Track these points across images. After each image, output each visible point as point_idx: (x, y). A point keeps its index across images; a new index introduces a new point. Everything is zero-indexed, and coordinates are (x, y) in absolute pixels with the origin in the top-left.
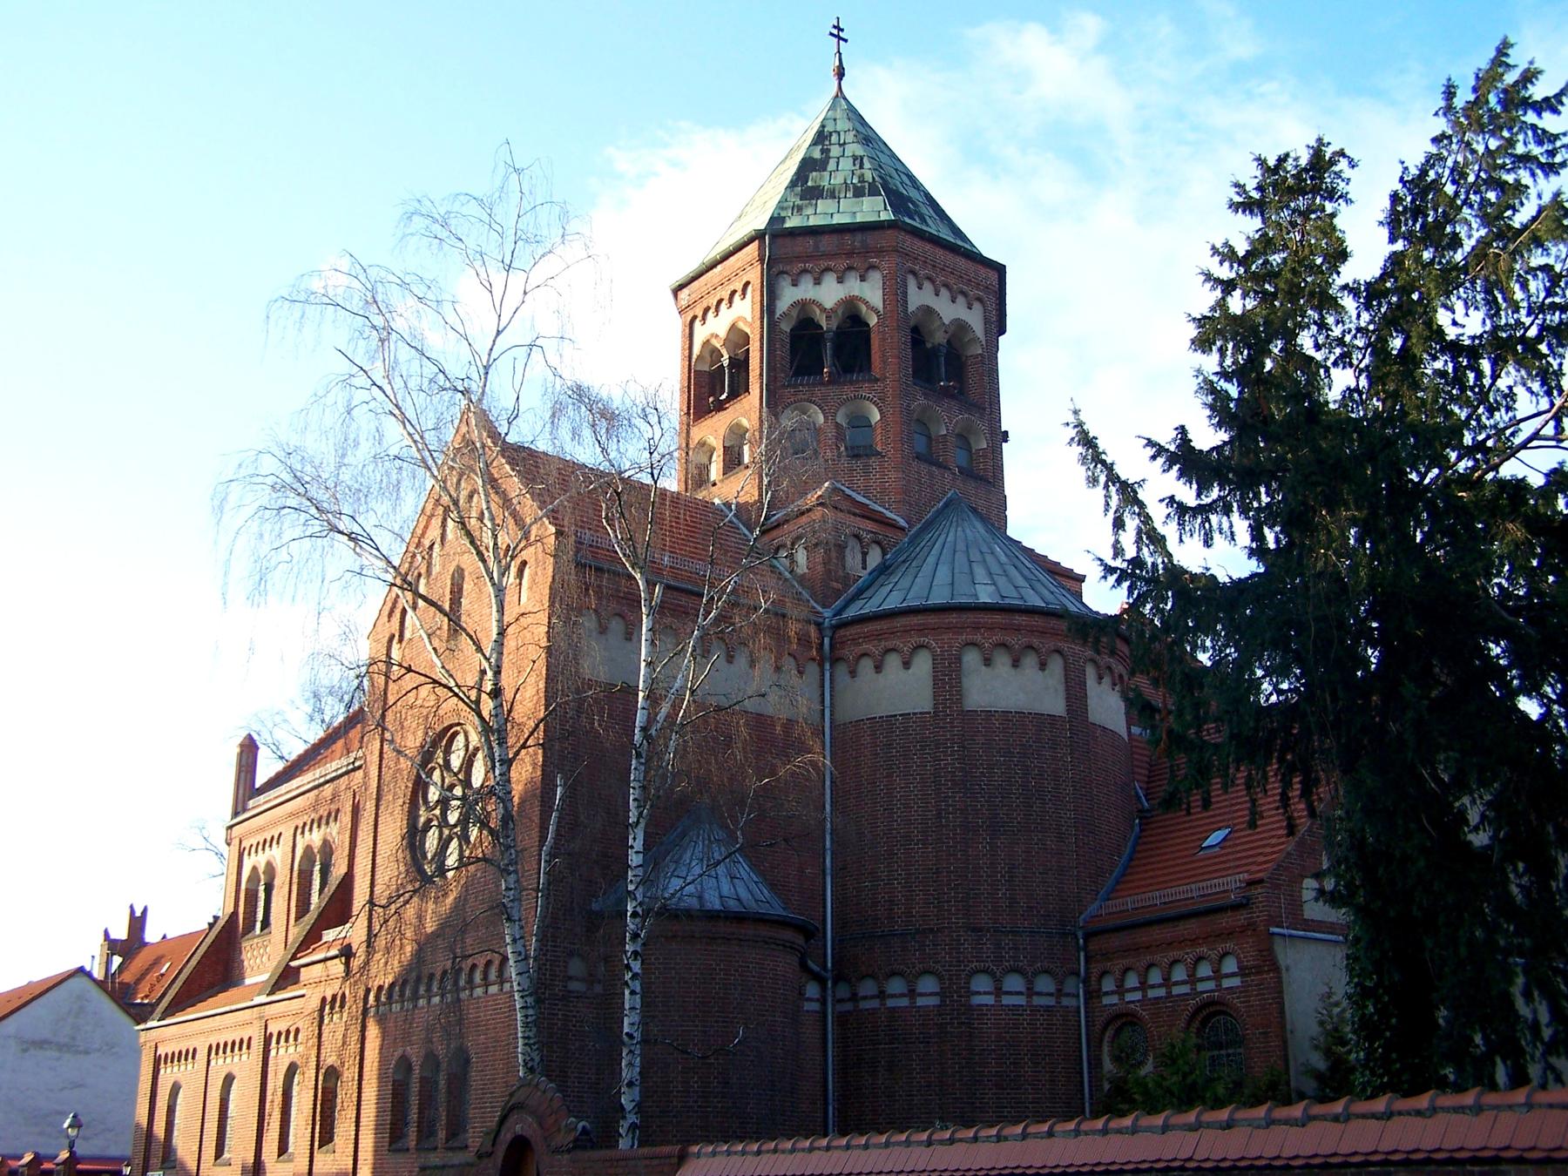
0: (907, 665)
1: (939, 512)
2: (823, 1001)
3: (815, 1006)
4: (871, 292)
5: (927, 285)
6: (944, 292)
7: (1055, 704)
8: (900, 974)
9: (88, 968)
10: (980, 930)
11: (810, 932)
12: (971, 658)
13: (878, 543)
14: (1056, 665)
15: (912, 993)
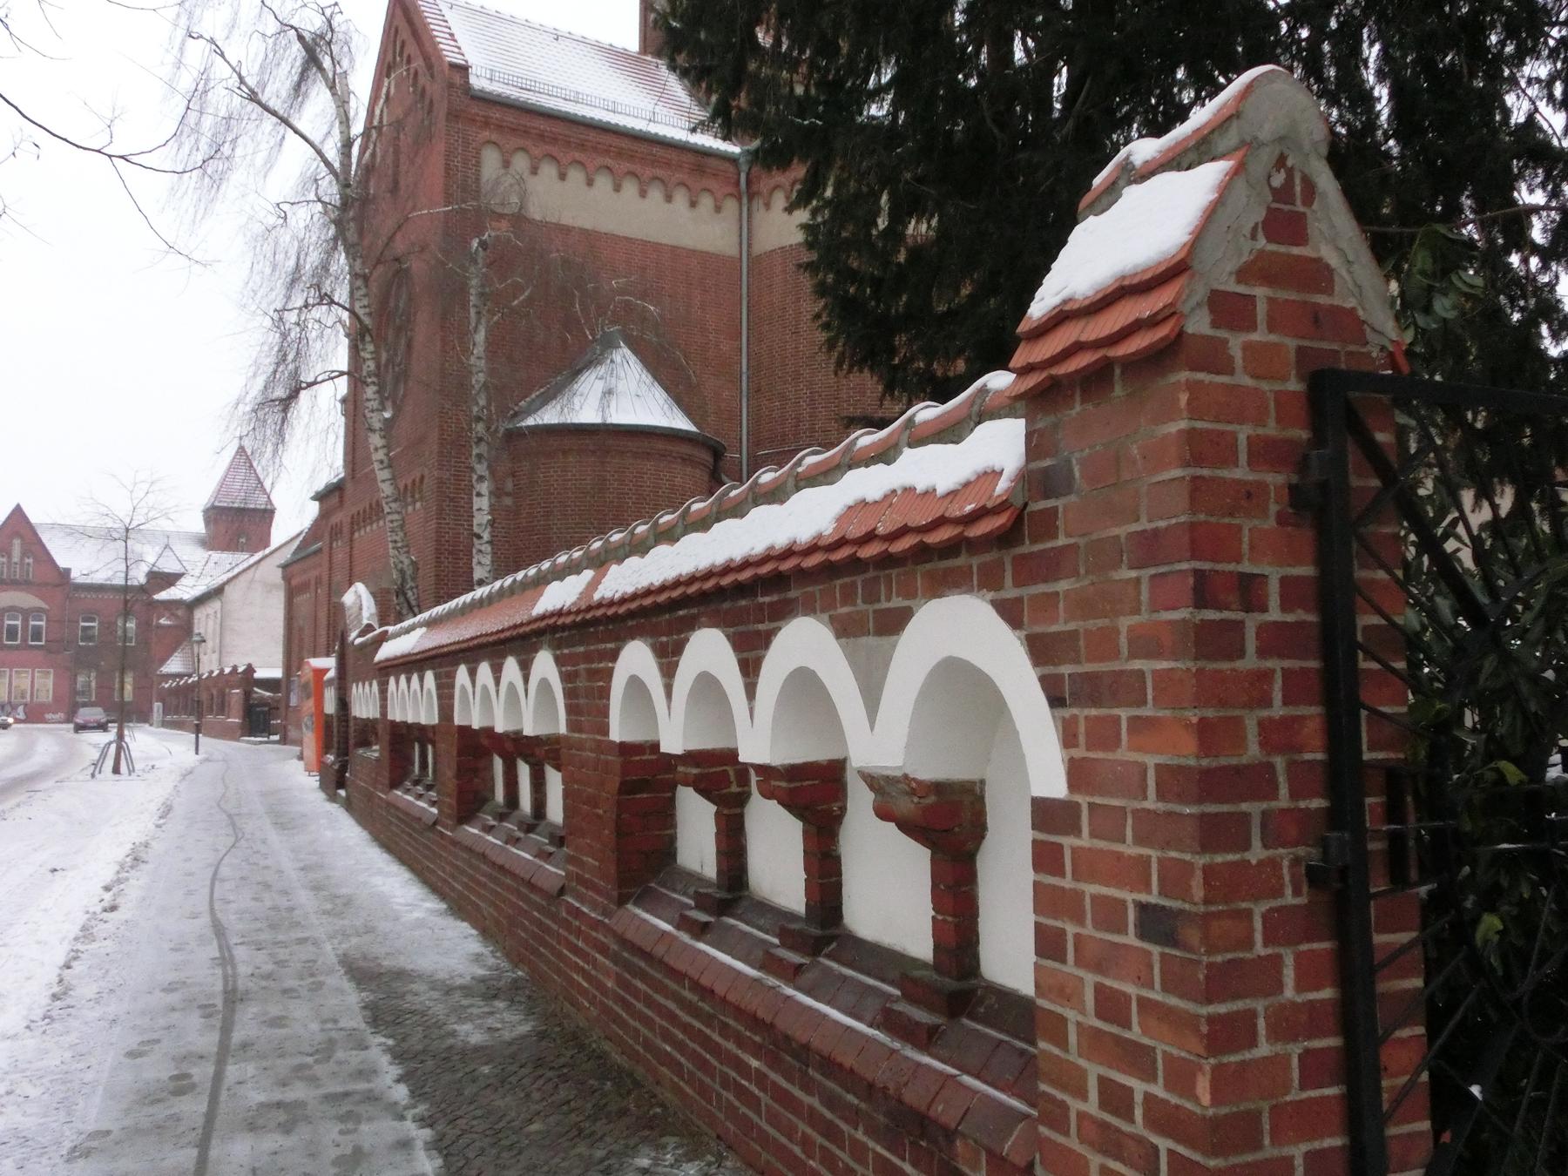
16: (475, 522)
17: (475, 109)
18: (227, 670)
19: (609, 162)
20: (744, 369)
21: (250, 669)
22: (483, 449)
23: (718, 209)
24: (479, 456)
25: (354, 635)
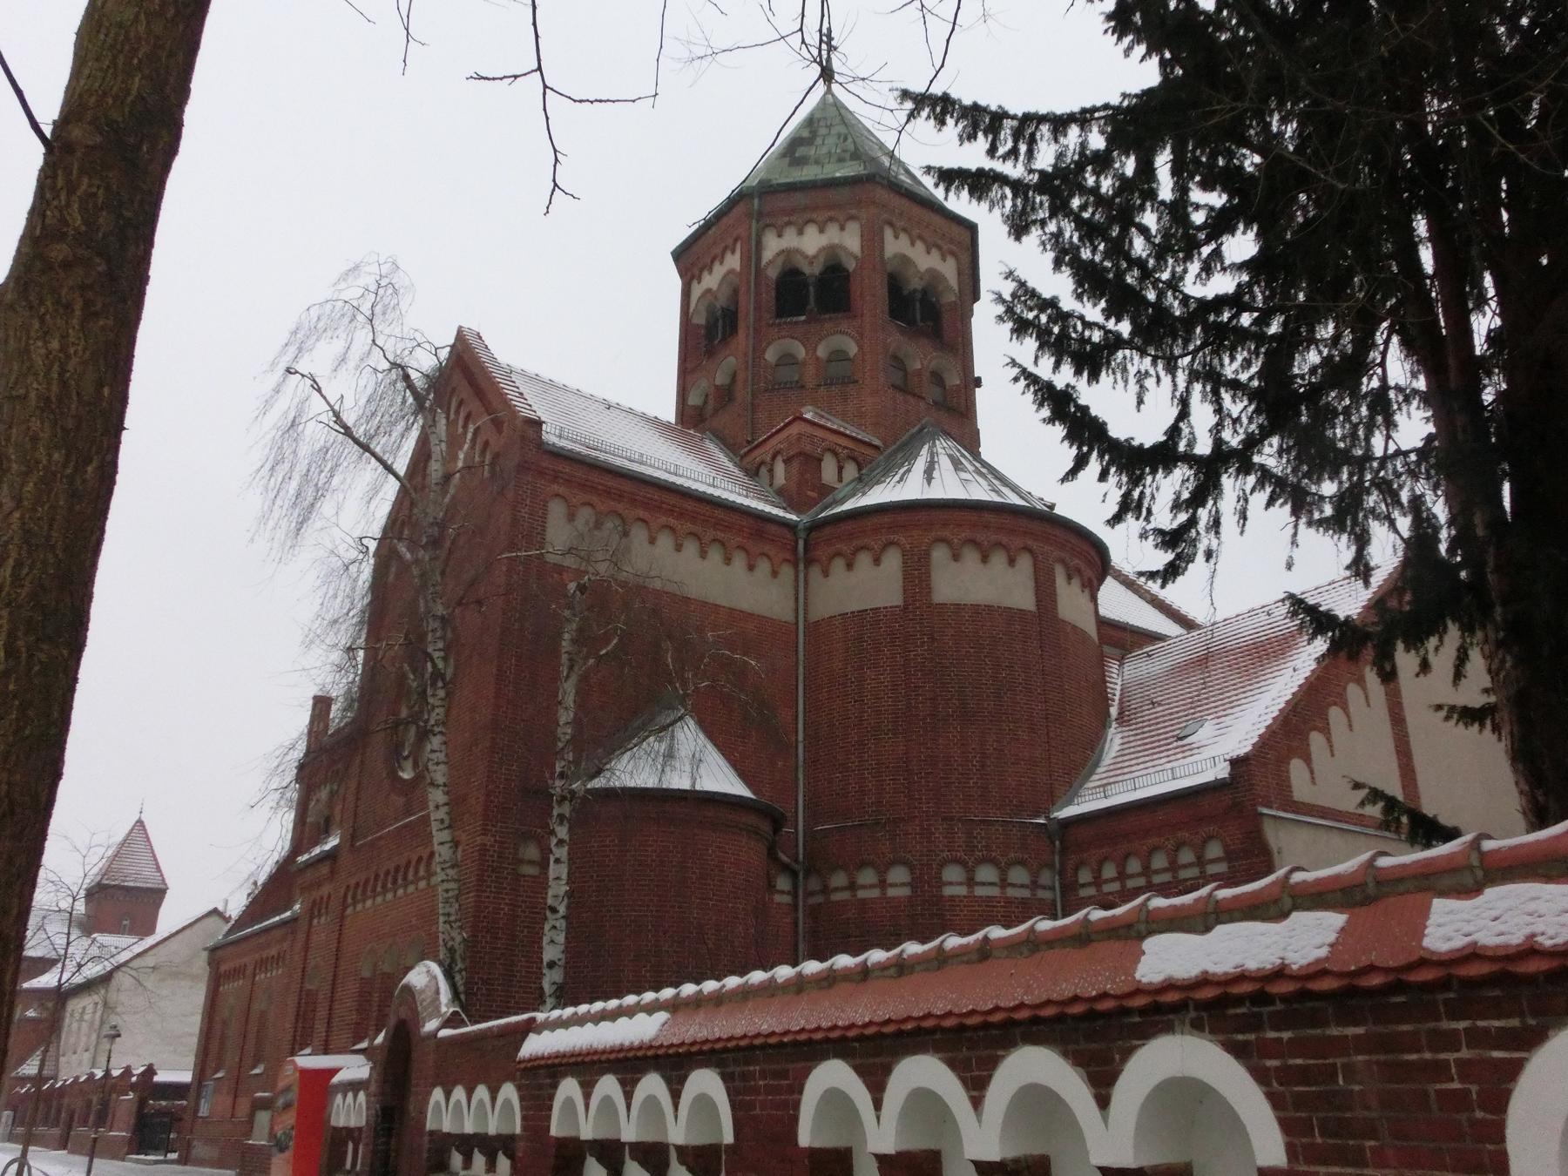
0: (877, 561)
1: (913, 437)
2: (795, 894)
3: (786, 899)
4: (850, 240)
5: (903, 236)
6: (919, 244)
7: (1023, 598)
8: (871, 864)
9: (221, 909)
10: (952, 819)
11: (777, 821)
12: (940, 554)
13: (854, 459)
14: (1025, 563)
15: (883, 884)
16: (550, 893)
17: (546, 463)
18: (116, 1073)
19: (672, 521)
20: (801, 738)
21: (150, 1071)
22: (566, 809)
23: (775, 574)
24: (561, 817)
25: (431, 1026)
